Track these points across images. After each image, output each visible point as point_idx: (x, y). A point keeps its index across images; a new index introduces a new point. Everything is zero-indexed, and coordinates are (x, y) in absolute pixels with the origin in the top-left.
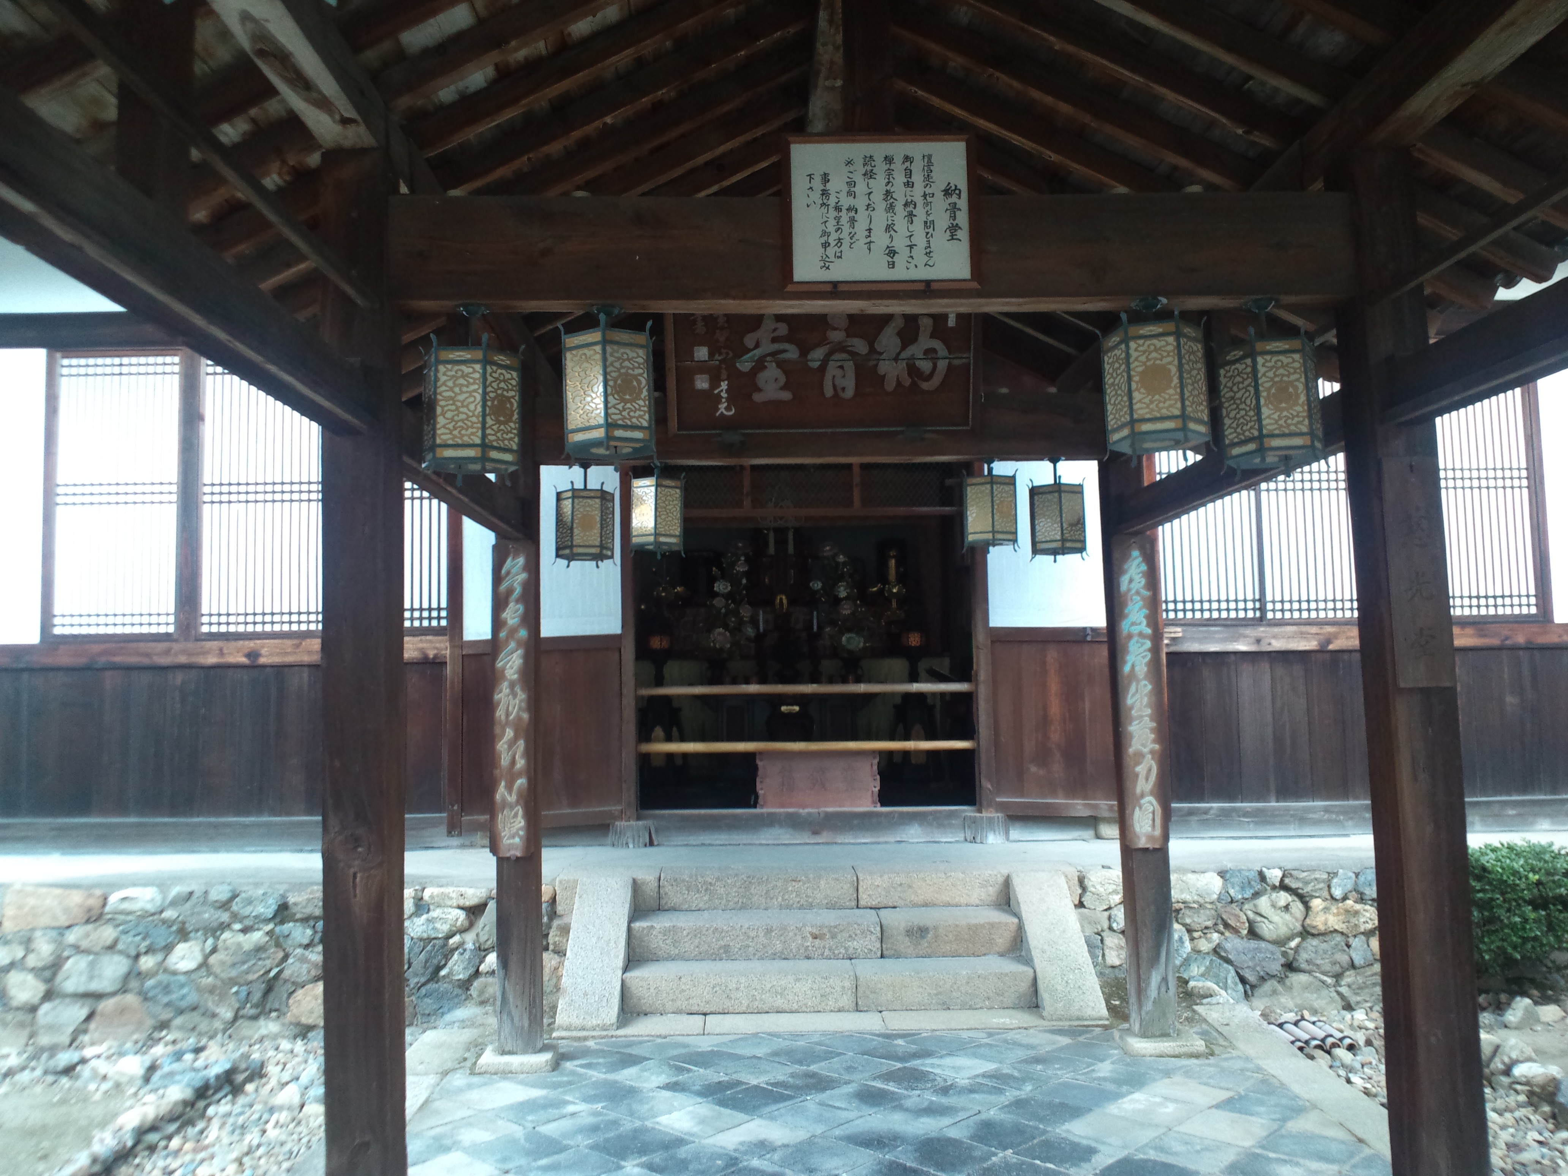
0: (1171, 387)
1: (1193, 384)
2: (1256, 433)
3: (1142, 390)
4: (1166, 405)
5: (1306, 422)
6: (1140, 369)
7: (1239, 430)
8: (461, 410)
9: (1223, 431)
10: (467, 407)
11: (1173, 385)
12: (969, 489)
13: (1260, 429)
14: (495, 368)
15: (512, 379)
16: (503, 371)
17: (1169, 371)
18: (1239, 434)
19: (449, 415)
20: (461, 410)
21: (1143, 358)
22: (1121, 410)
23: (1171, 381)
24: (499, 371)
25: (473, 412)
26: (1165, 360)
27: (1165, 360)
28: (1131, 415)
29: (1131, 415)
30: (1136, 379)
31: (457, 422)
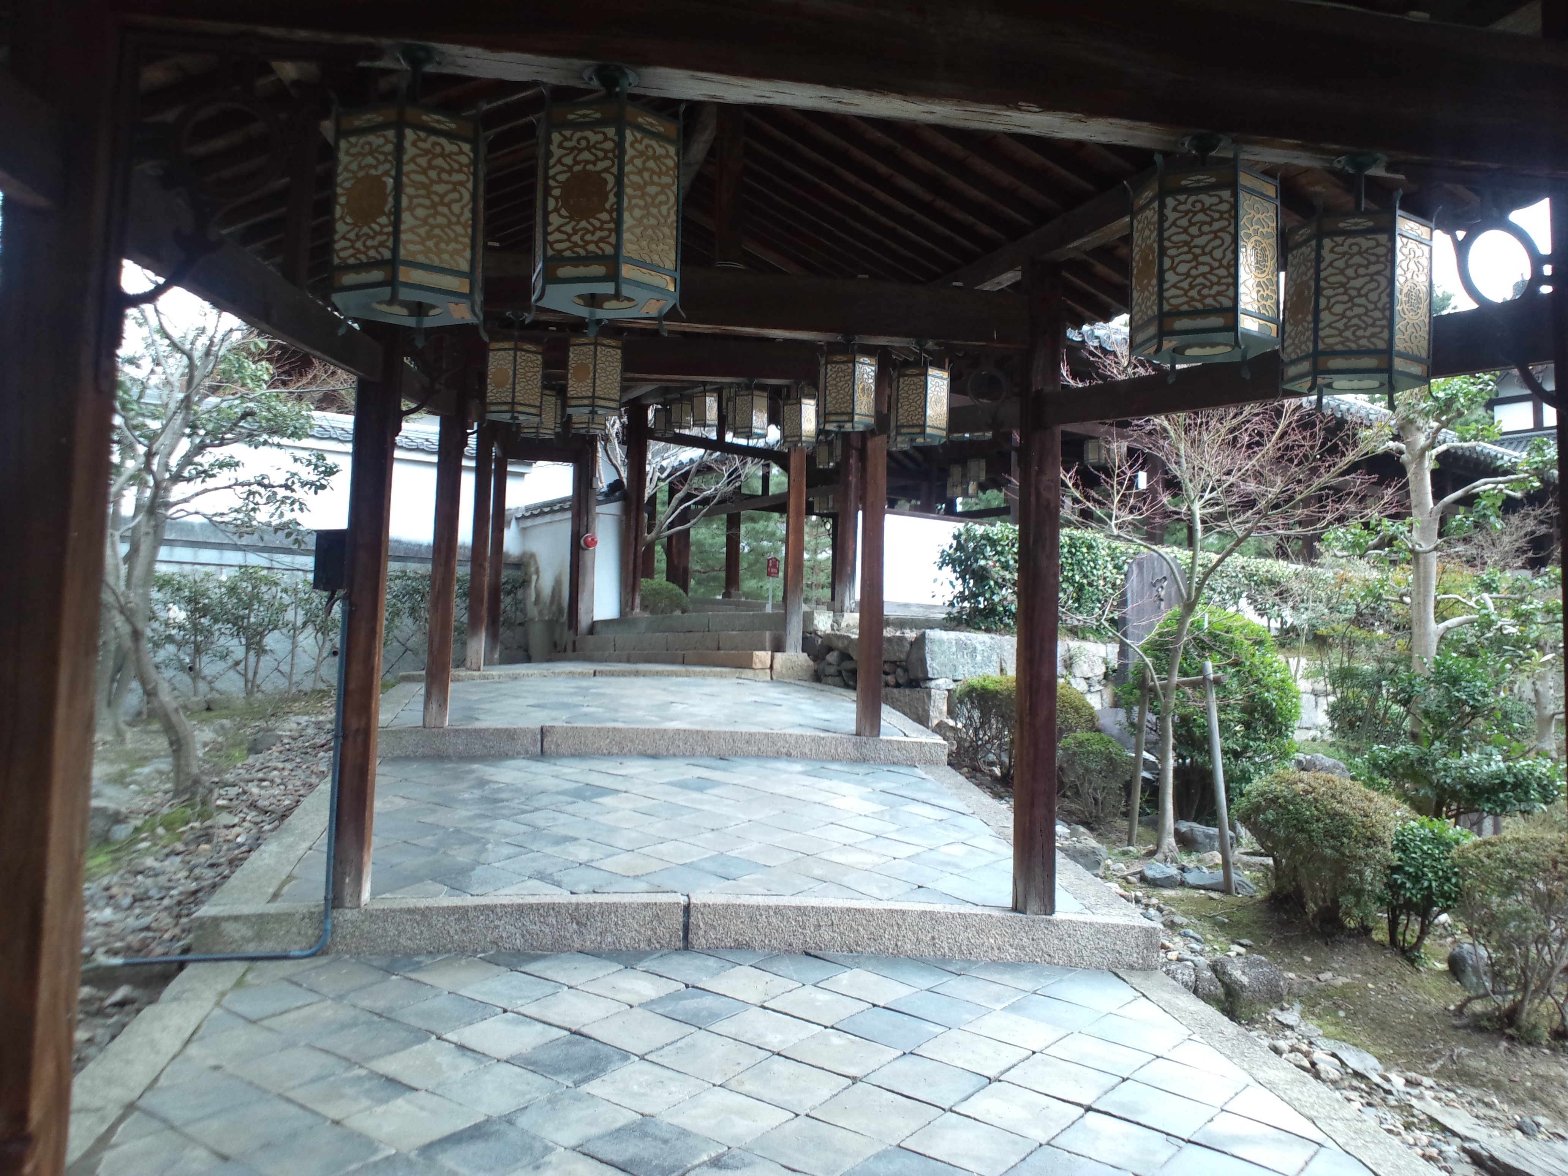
0: (602, 209)
1: (646, 207)
2: (387, 254)
3: (563, 212)
4: (1213, 291)
5: (468, 254)
6: (562, 178)
7: (359, 245)
8: (1202, 259)
9: (334, 242)
10: (449, 205)
11: (608, 206)
12: (491, 354)
13: (395, 250)
14: (639, 136)
15: (668, 156)
16: (654, 143)
17: (605, 181)
18: (359, 251)
19: (1183, 268)
20: (1202, 259)
21: (568, 160)
22: (1149, 298)
23: (606, 199)
24: (646, 141)
25: (1220, 261)
26: (601, 165)
27: (601, 165)
28: (1316, 338)
29: (1316, 338)
30: (556, 192)
31: (1350, 319)
